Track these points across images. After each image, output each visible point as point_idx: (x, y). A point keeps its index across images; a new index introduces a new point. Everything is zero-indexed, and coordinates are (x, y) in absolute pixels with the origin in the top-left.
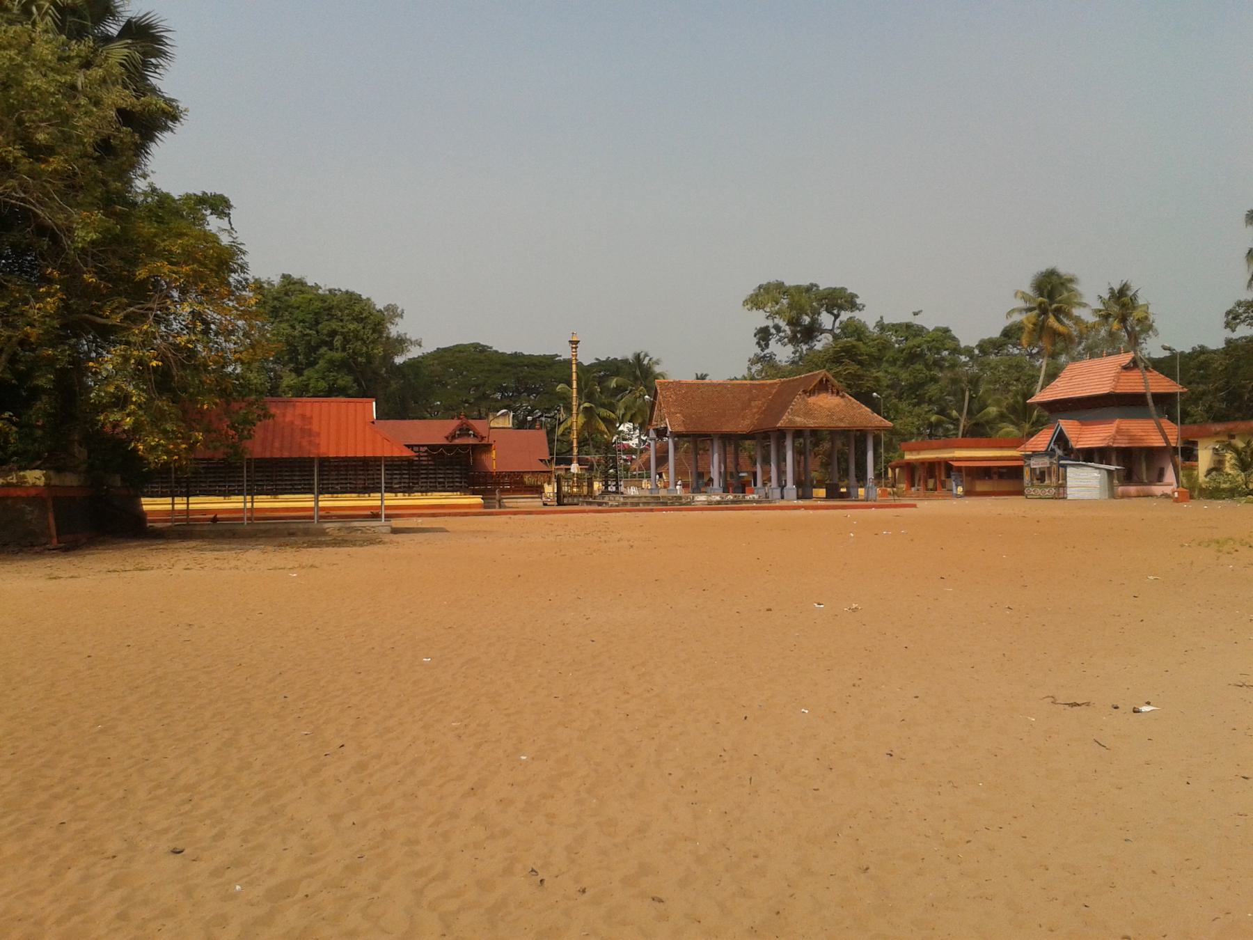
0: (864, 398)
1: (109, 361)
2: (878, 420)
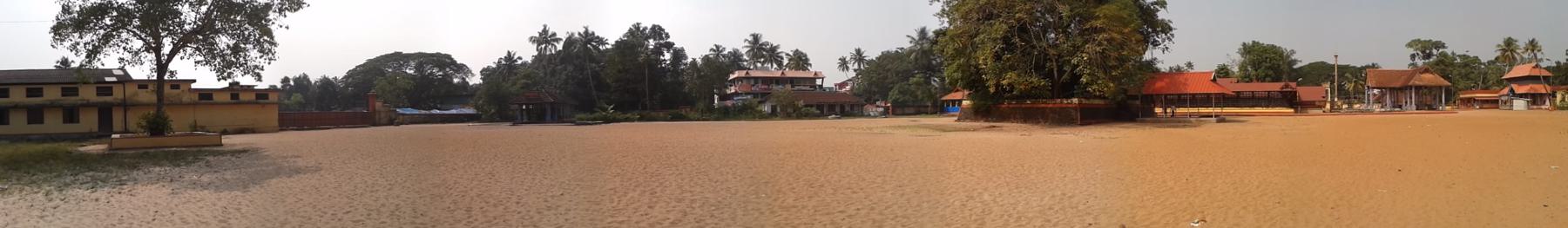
0: (1446, 77)
2: (1446, 83)
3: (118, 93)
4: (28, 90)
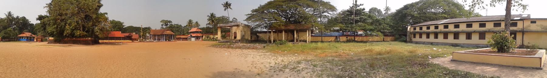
1: (96, 28)
3: (520, 26)
4: (480, 24)
